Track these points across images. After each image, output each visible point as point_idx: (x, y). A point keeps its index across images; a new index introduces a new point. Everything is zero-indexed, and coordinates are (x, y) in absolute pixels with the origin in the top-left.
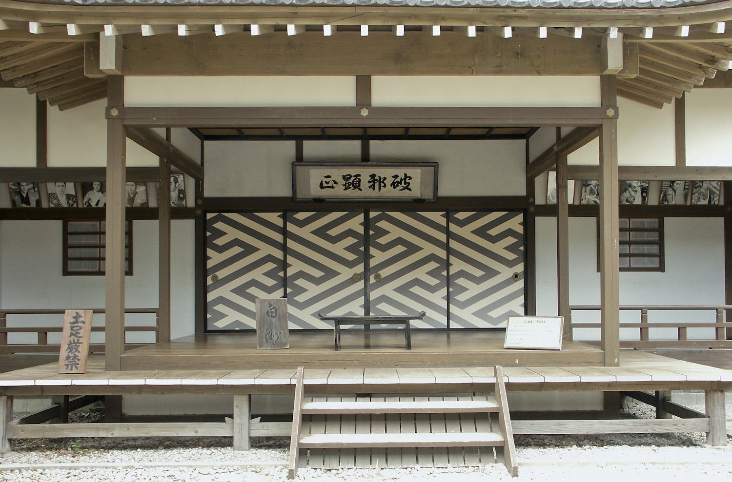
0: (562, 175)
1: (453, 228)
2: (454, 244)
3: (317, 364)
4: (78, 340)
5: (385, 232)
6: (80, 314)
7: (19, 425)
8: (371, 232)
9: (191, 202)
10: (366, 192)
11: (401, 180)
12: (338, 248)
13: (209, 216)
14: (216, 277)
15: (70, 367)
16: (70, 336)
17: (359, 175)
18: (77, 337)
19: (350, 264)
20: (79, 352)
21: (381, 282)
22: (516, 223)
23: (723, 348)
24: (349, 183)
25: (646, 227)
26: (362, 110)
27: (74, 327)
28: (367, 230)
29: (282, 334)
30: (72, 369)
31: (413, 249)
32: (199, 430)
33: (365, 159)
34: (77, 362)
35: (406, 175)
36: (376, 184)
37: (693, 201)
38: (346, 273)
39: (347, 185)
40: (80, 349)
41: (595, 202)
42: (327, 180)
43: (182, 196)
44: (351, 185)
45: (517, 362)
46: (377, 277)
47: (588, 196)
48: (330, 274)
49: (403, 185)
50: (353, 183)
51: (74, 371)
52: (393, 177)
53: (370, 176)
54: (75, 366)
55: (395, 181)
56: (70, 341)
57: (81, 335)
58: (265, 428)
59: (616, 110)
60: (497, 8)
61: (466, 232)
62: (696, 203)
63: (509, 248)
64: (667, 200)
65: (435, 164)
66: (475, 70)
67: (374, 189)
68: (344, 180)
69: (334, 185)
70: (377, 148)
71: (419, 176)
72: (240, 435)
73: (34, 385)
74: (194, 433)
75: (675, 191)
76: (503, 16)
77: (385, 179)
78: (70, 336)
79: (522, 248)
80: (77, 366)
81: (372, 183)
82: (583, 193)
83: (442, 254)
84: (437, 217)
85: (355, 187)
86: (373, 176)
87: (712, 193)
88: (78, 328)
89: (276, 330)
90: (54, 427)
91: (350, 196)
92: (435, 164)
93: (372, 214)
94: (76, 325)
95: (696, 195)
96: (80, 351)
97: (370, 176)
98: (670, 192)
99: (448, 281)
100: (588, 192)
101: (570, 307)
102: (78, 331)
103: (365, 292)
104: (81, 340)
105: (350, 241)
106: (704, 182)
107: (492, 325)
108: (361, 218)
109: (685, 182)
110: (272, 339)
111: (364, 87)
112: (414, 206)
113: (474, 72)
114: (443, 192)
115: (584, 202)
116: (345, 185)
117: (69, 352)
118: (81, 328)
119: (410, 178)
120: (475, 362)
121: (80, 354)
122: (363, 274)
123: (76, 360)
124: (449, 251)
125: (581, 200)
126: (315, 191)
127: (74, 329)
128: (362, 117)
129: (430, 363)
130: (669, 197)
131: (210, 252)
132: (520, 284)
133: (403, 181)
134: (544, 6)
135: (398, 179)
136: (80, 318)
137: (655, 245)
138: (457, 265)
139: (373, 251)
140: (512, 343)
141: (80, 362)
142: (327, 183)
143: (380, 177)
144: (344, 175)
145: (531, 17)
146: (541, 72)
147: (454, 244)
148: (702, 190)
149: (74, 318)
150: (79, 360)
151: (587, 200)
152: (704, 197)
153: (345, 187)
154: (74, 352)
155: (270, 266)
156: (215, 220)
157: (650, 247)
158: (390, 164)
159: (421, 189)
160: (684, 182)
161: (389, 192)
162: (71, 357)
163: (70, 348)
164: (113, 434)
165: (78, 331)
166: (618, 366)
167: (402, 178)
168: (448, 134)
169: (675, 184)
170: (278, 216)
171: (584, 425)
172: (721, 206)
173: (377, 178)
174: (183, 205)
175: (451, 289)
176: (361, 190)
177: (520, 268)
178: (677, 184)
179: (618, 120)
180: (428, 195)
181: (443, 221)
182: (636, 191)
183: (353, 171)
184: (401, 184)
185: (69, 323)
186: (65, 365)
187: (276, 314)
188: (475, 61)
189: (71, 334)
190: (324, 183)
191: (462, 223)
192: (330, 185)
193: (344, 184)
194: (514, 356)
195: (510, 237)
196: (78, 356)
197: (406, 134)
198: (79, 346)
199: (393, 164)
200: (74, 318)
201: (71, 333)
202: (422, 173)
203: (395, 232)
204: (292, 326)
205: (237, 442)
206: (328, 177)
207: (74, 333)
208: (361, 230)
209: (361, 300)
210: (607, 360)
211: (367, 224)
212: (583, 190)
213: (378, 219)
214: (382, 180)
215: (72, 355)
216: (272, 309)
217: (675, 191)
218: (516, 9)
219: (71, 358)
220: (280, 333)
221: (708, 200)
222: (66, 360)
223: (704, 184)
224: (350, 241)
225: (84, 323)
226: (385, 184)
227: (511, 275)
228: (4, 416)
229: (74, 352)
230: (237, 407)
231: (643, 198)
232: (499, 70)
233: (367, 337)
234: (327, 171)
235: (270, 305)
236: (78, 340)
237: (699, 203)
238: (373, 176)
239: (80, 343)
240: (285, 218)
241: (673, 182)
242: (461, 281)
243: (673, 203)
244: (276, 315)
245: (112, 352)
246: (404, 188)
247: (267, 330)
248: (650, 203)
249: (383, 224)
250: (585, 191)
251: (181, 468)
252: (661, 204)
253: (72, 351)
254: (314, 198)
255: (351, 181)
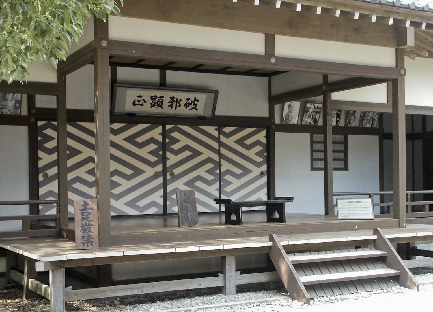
0: (328, 106)
1: (223, 139)
2: (223, 151)
3: (245, 234)
4: (89, 223)
5: (177, 141)
6: (87, 202)
7: (72, 291)
8: (167, 141)
9: (24, 112)
10: (166, 110)
11: (192, 102)
12: (144, 152)
13: (40, 123)
14: (46, 175)
15: (86, 244)
16: (82, 220)
17: (163, 97)
18: (88, 220)
19: (153, 165)
20: (92, 232)
21: (175, 178)
22: (262, 136)
23: (411, 217)
24: (154, 102)
25: (337, 141)
26: (102, 42)
27: (85, 213)
28: (164, 139)
29: (194, 215)
30: (88, 246)
31: (196, 153)
32: (202, 283)
33: (163, 85)
34: (92, 240)
35: (195, 98)
36: (174, 104)
37: (363, 124)
38: (150, 171)
39: (153, 103)
40: (92, 230)
41: (310, 123)
42: (139, 99)
43: (18, 105)
44: (155, 104)
45: (356, 227)
46: (172, 174)
47: (307, 119)
48: (138, 172)
49: (192, 105)
50: (157, 103)
51: (90, 247)
52: (186, 99)
53: (170, 98)
54: (91, 244)
55: (187, 103)
56: (83, 224)
57: (91, 219)
58: (244, 277)
59: (405, 70)
60: (393, 6)
61: (230, 141)
62: (364, 126)
63: (151, 153)
64: (350, 124)
65: (216, 92)
66: (333, 38)
67: (172, 108)
68: (152, 100)
69: (144, 103)
70: (172, 76)
71: (204, 100)
72: (230, 284)
73: (123, 255)
74: (199, 286)
75: (355, 118)
76: (388, 11)
77: (181, 100)
78: (82, 220)
79: (265, 154)
80: (91, 243)
81: (171, 103)
82: (304, 117)
83: (216, 157)
84: (212, 130)
85: (159, 106)
86: (173, 98)
87: (374, 120)
88: (88, 214)
89: (190, 212)
90: (99, 290)
91: (154, 112)
92: (216, 92)
93: (168, 127)
94: (86, 211)
95: (366, 120)
96: (93, 231)
97: (170, 98)
98: (353, 118)
99: (220, 178)
100: (307, 116)
101: (334, 194)
102: (88, 216)
103: (164, 185)
104: (92, 223)
105: (152, 147)
106: (371, 113)
107: (209, 210)
108: (159, 129)
109: (362, 112)
110: (188, 219)
111: (270, 42)
112: (197, 122)
113: (333, 39)
114: (219, 112)
115: (303, 123)
116: (151, 104)
117: (83, 233)
118: (90, 214)
119: (198, 101)
120: (335, 228)
121: (93, 234)
122: (162, 173)
123: (90, 239)
124: (221, 156)
125: (301, 123)
126: (129, 107)
127: (84, 214)
128: (271, 64)
129: (310, 230)
130: (351, 122)
131: (41, 154)
132: (264, 179)
133: (193, 103)
134: (415, 9)
135: (190, 101)
136: (88, 205)
137: (342, 153)
138: (225, 166)
139: (169, 155)
140: (343, 216)
141: (94, 240)
142: (139, 101)
143: (177, 99)
144: (152, 96)
145: (402, 13)
146: (368, 43)
147: (223, 151)
148: (369, 118)
149: (83, 206)
150: (93, 238)
151: (306, 121)
152: (369, 122)
153: (152, 105)
154: (88, 232)
155: (210, 166)
156: (45, 127)
157: (339, 155)
158: (176, 89)
159: (204, 109)
160: (360, 112)
161: (182, 111)
162: (85, 236)
163: (84, 230)
164: (143, 292)
165: (88, 216)
166: (406, 228)
167: (193, 101)
168: (225, 70)
169: (356, 113)
170: (215, 129)
171: (412, 263)
172: (377, 128)
173: (175, 99)
174: (18, 113)
175: (222, 183)
176: (162, 108)
177: (264, 168)
178: (357, 113)
179: (405, 76)
180: (208, 114)
181: (216, 134)
182: (334, 117)
183: (158, 93)
184: (191, 105)
185: (79, 210)
186: (82, 243)
187: (189, 200)
188: (333, 31)
189: (83, 219)
190: (136, 101)
191: (228, 135)
192: (140, 103)
193: (151, 103)
194: (355, 224)
195: (152, 144)
196: (91, 236)
197: (197, 68)
198: (91, 227)
199: (188, 89)
200: (83, 206)
201: (82, 217)
202: (206, 98)
203: (184, 141)
204: (113, 214)
205: (228, 290)
206: (140, 97)
207: (85, 218)
208: (160, 138)
209: (161, 192)
210: (401, 225)
211: (164, 134)
212: (305, 115)
213: (172, 130)
214: (178, 101)
215: (86, 235)
216: (186, 197)
217: (355, 118)
218: (399, 8)
219: (86, 237)
220: (193, 214)
221: (371, 123)
222: (82, 239)
223: (370, 114)
224: (152, 147)
225: (92, 209)
226: (180, 104)
227: (259, 173)
228: (63, 284)
229: (88, 232)
230: (228, 264)
231: (337, 121)
232: (346, 39)
233: (165, 221)
234: (140, 92)
235: (185, 195)
236: (89, 223)
237: (366, 126)
238: (173, 98)
239: (91, 225)
240: (220, 132)
241: (355, 112)
242: (228, 177)
243: (353, 125)
244: (189, 201)
245: (105, 232)
246: (193, 108)
247: (185, 212)
248: (340, 125)
249: (176, 135)
250: (306, 116)
251: (225, 307)
252: (346, 126)
253: (85, 232)
254: (127, 112)
255: (156, 101)
